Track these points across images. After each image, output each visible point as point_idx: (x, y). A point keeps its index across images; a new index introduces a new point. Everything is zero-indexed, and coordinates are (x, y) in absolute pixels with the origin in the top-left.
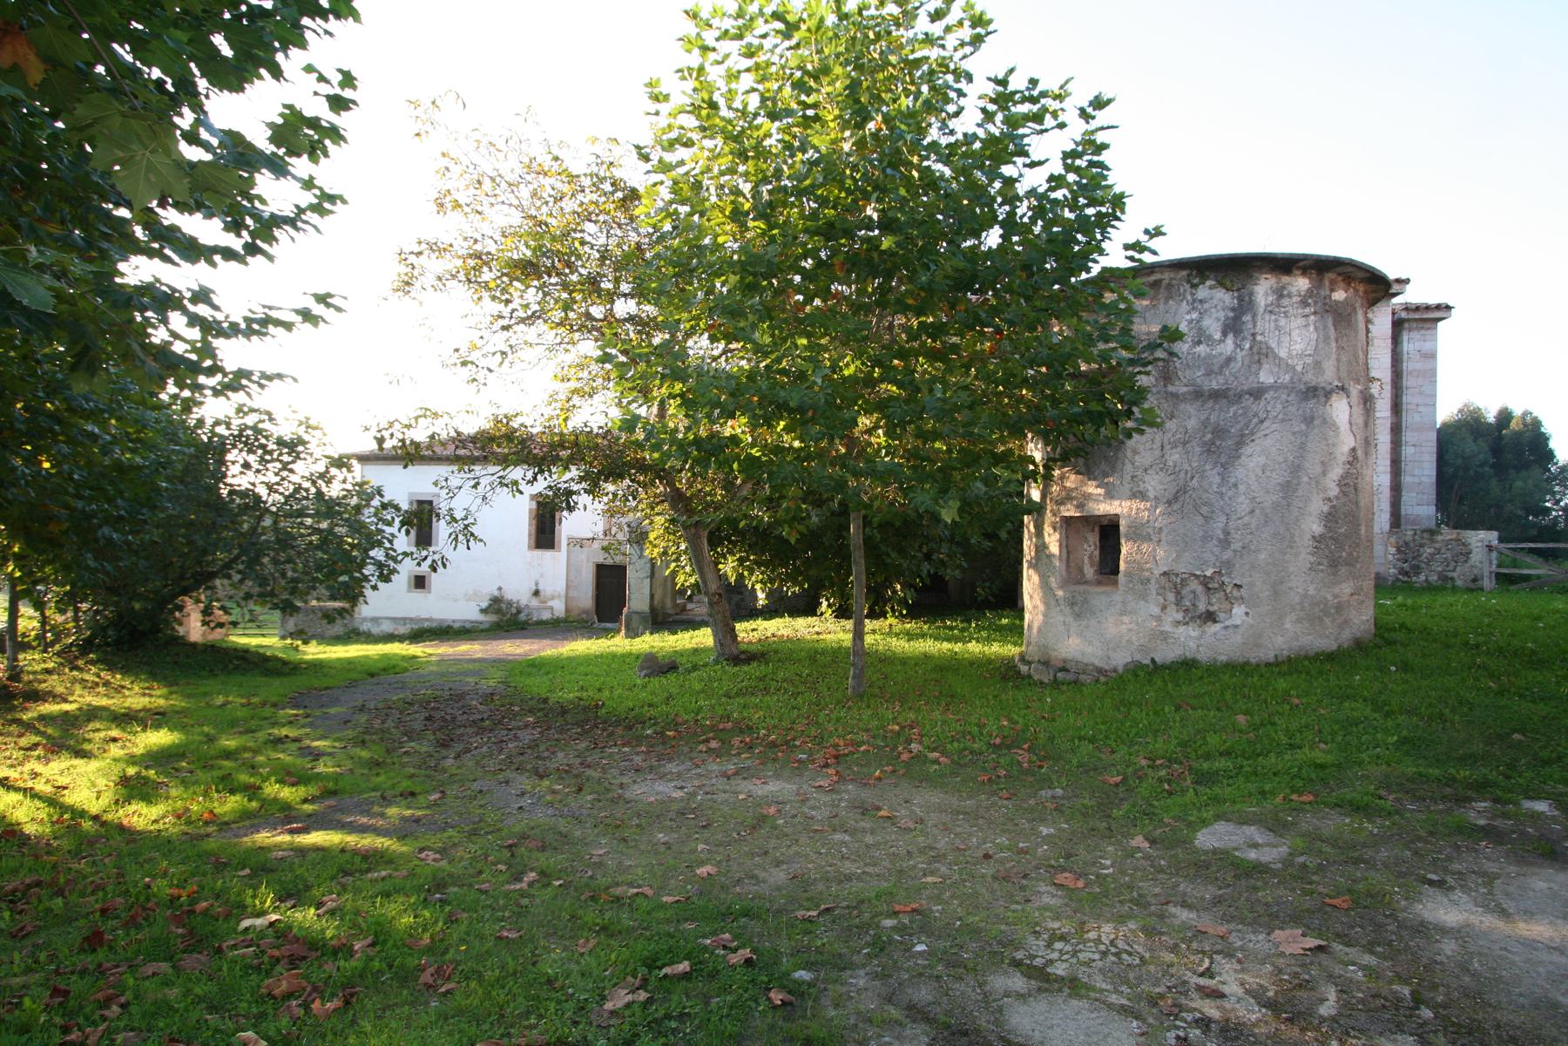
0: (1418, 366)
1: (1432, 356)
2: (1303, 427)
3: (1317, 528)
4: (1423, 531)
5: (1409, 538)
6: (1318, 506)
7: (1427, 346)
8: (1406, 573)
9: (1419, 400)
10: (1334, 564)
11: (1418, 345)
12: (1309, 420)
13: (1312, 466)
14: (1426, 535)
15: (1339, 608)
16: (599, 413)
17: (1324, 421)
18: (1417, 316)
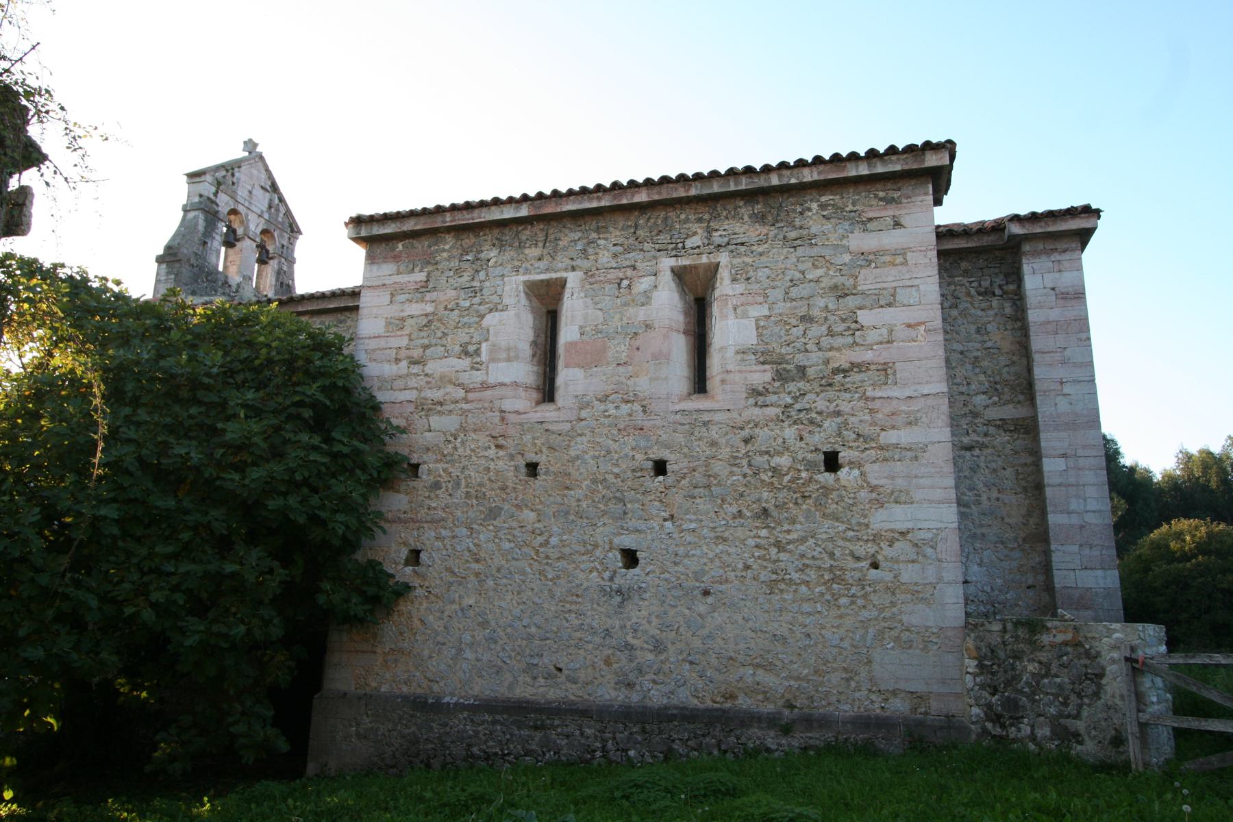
0: (1054, 314)
1: (1077, 295)
4: (1017, 624)
5: (995, 639)
7: (1065, 280)
8: (997, 719)
9: (1061, 373)
11: (1050, 279)
14: (1021, 632)
16: (1098, 508)
18: (1037, 229)
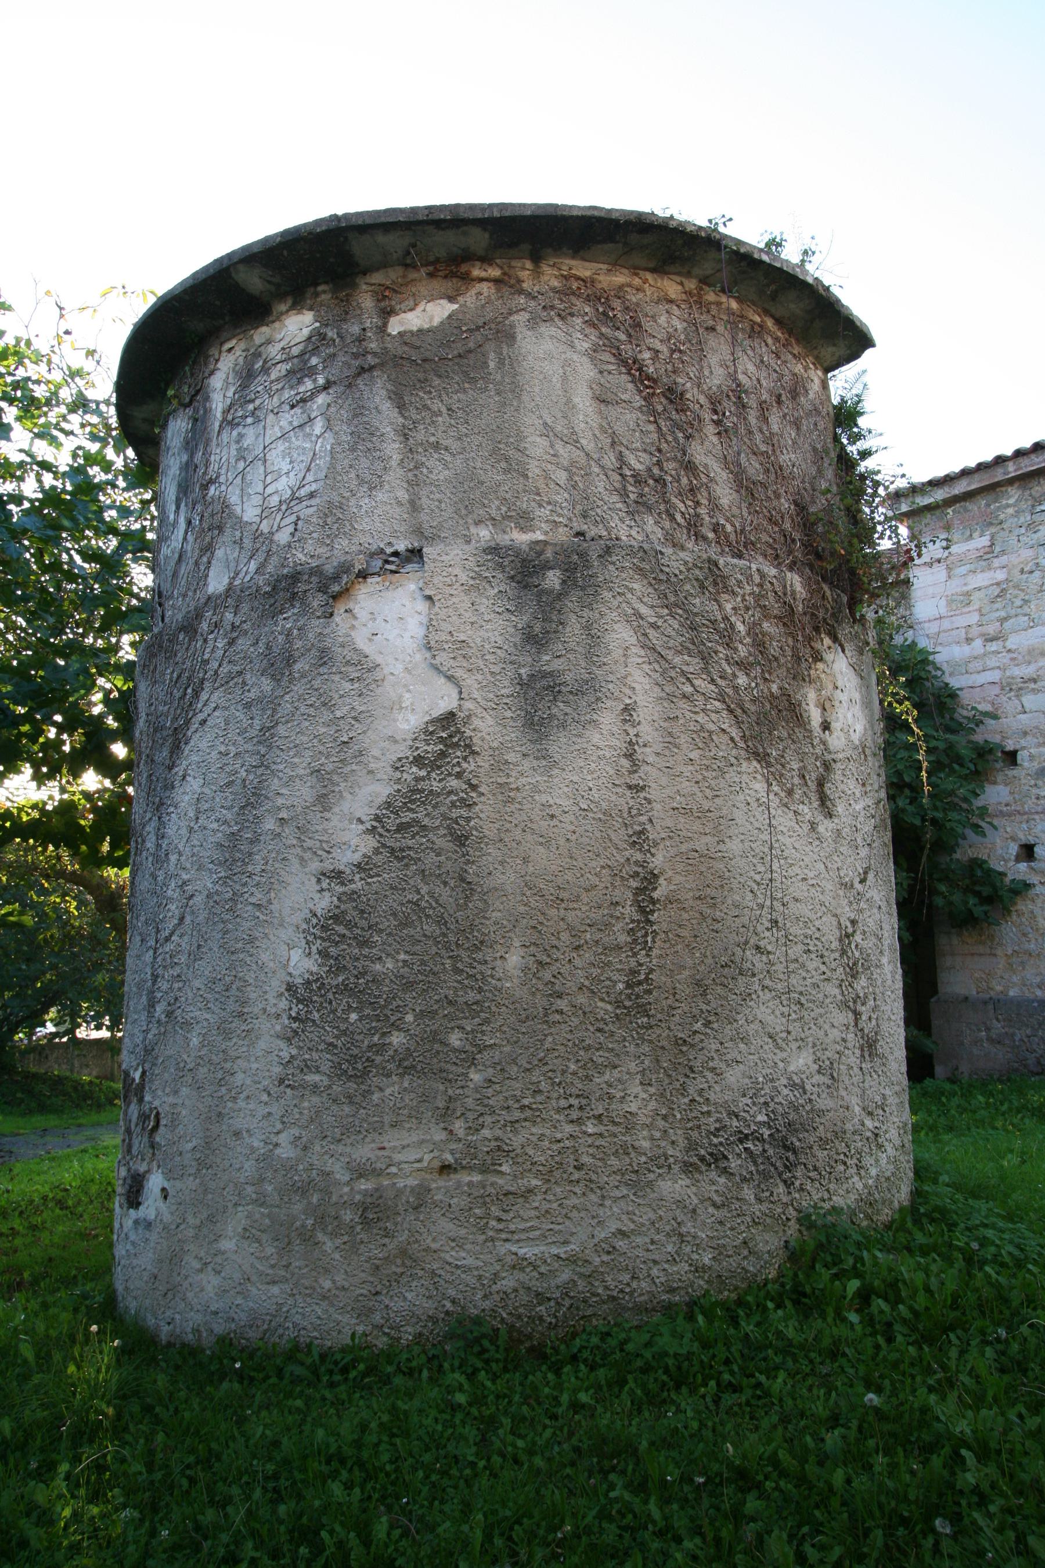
2: (266, 684)
3: (301, 963)
6: (300, 896)
10: (356, 1068)
12: (280, 665)
13: (294, 793)
15: (374, 1213)
17: (324, 657)
